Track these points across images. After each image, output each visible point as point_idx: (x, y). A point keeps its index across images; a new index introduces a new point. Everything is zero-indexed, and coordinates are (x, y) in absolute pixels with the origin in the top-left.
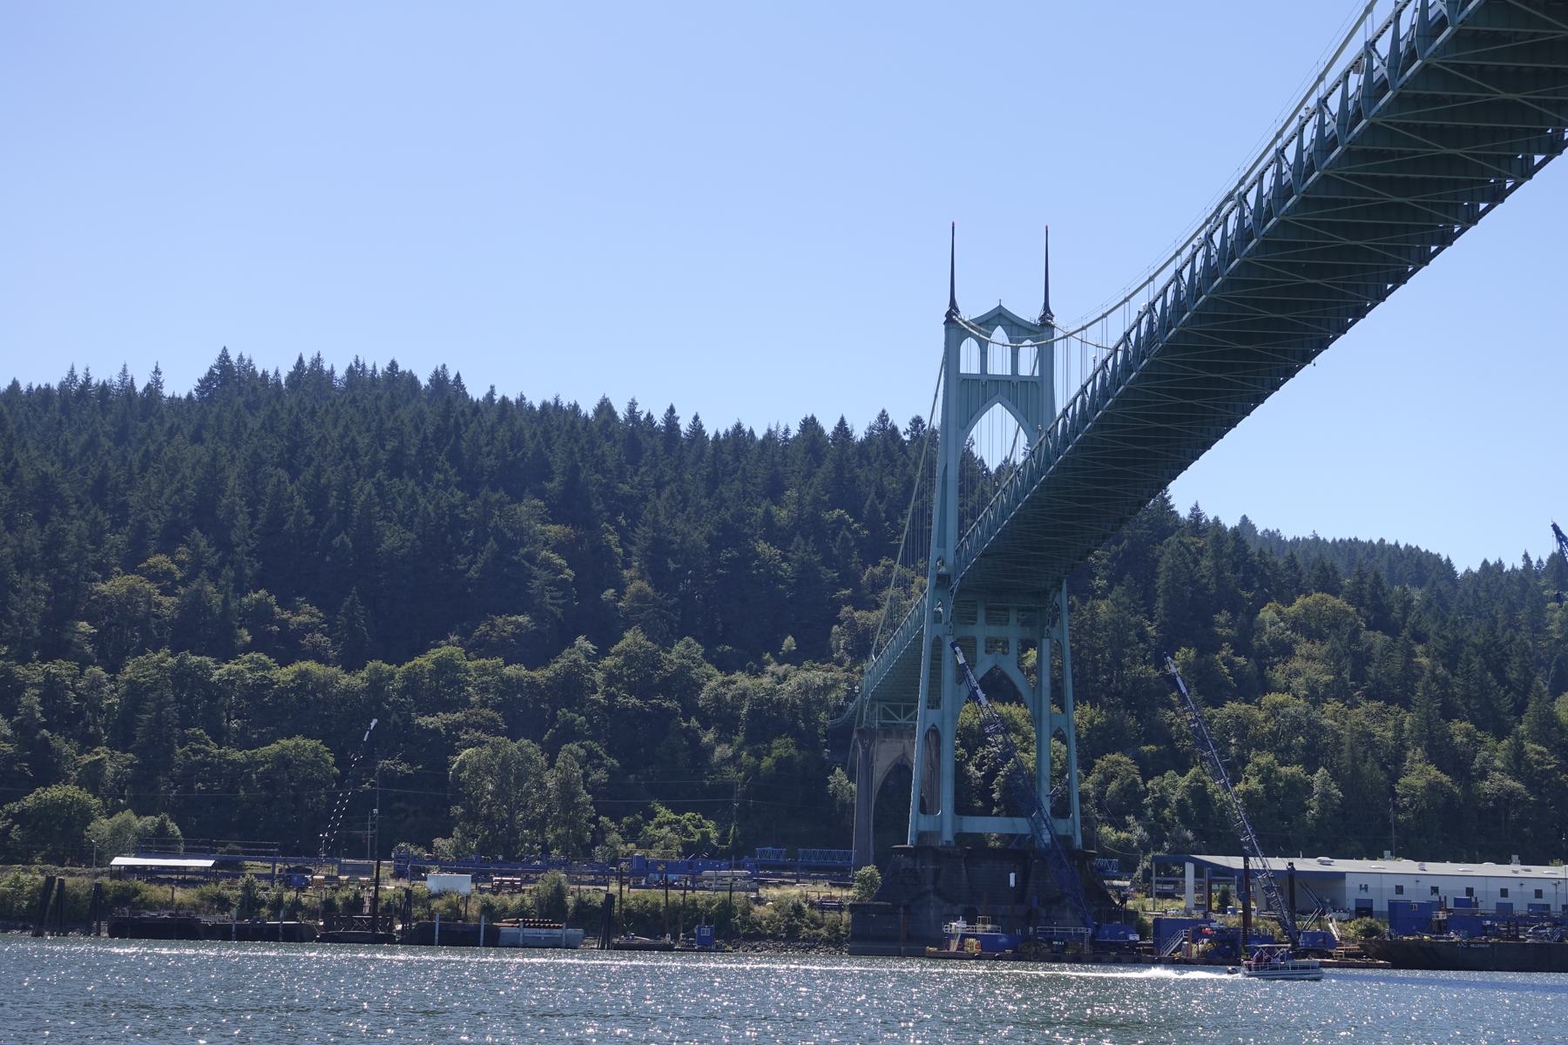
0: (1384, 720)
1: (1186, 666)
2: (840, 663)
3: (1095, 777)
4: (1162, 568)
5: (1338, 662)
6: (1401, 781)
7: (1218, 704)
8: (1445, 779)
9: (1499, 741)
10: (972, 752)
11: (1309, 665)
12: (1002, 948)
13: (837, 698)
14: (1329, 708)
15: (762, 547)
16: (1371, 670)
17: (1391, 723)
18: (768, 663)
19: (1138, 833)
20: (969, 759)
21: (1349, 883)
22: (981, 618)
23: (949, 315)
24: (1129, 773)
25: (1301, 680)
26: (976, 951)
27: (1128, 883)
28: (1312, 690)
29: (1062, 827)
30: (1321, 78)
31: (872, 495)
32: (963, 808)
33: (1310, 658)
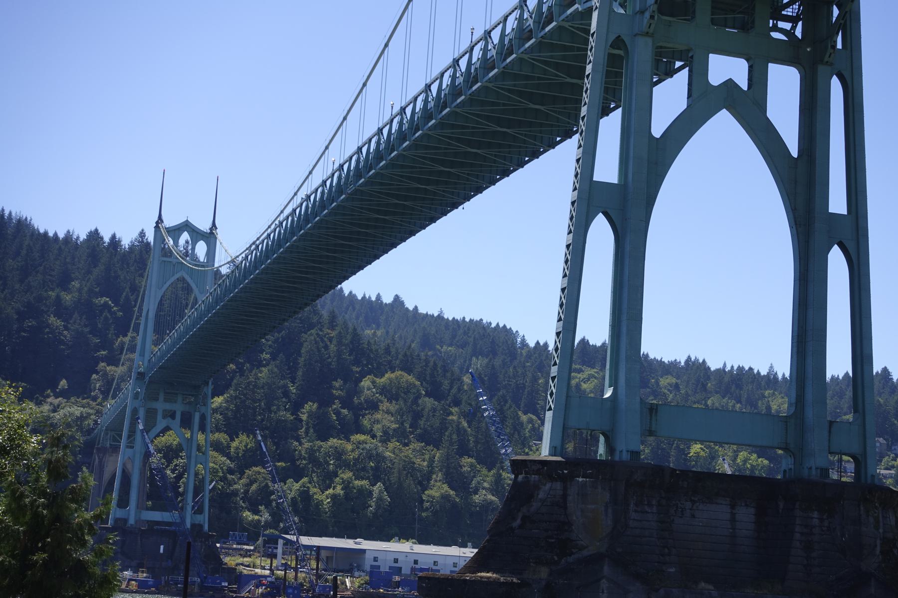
0: (423, 454)
1: (311, 415)
2: (95, 399)
3: (244, 481)
4: (303, 351)
5: (402, 416)
6: (426, 492)
7: (325, 439)
8: (452, 493)
9: (489, 471)
10: (169, 462)
11: (384, 418)
12: (149, 587)
13: (89, 425)
14: (391, 445)
15: (52, 319)
16: (422, 423)
17: (427, 457)
18: (48, 396)
19: (266, 516)
20: (167, 466)
21: (369, 557)
22: (161, 397)
23: (157, 223)
24: (265, 479)
25: (379, 426)
26: (135, 588)
27: (252, 548)
28: (385, 433)
29: (199, 519)
30: (282, 212)
31: (127, 290)
32: (140, 507)
33: (388, 412)
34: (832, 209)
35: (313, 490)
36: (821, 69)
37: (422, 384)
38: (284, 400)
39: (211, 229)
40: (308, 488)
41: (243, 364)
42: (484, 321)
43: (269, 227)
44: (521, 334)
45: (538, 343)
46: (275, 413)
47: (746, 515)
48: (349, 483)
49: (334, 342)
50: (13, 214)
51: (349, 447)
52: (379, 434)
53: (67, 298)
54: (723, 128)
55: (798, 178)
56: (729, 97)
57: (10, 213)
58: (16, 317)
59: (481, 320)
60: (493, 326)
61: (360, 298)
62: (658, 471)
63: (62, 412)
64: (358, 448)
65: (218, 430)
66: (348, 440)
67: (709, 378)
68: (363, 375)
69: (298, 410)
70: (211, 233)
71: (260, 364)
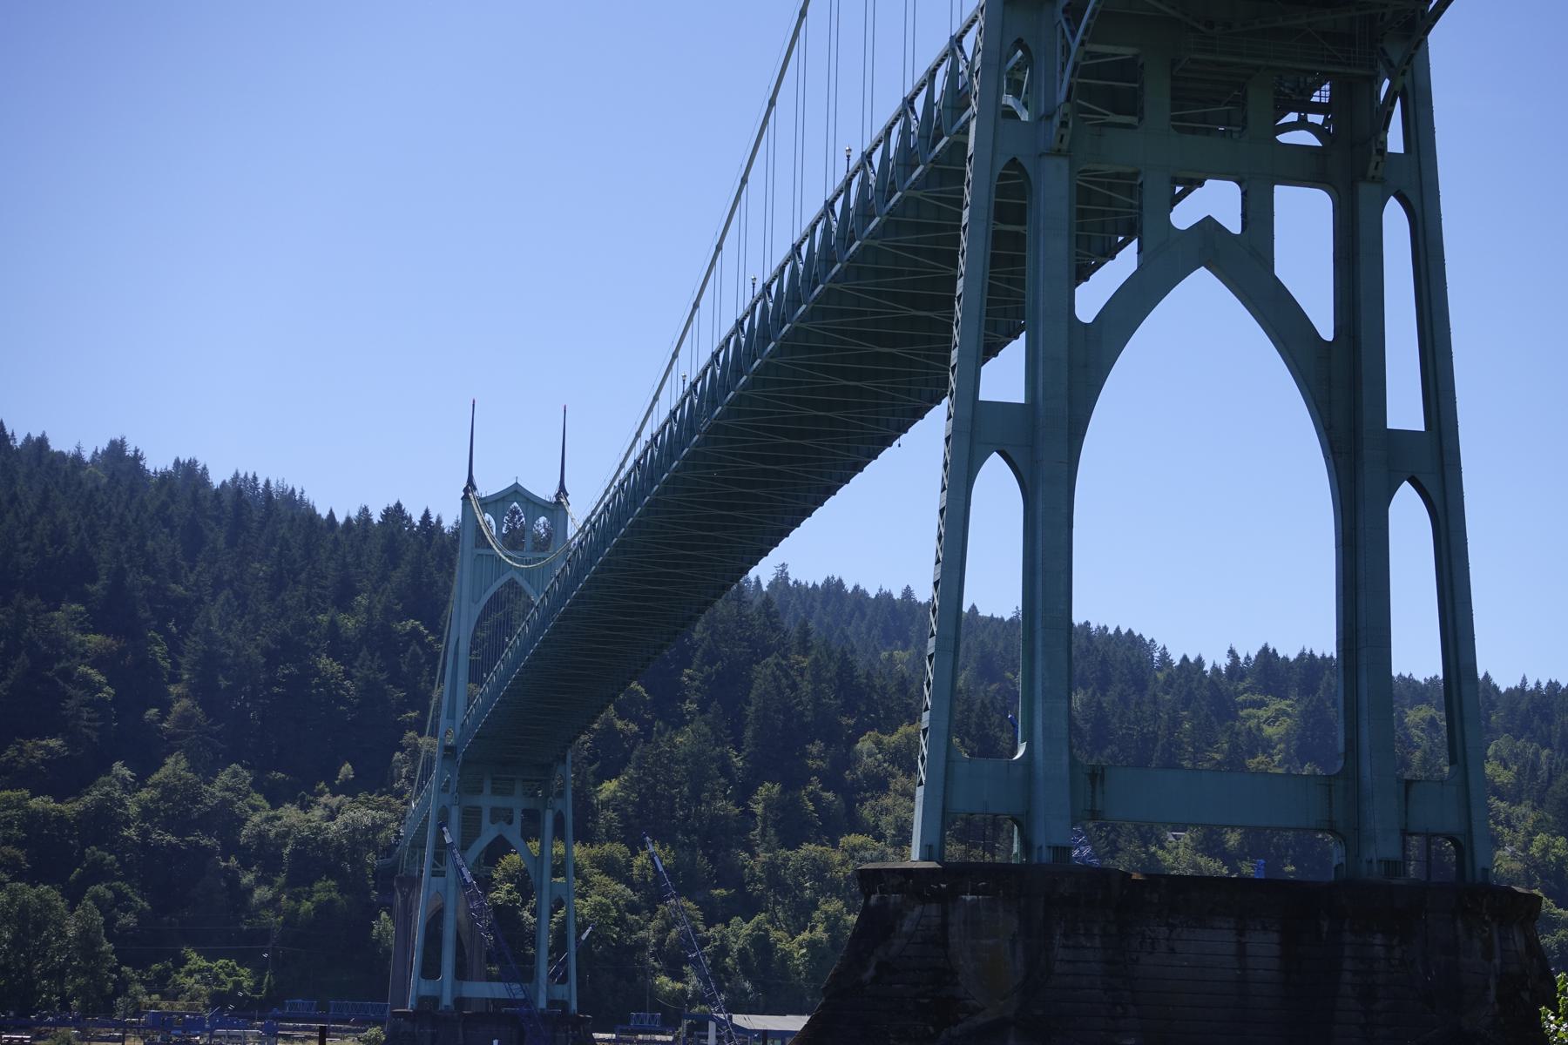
2: (399, 794)
7: (794, 845)
15: (324, 662)
18: (321, 793)
19: (693, 983)
20: (523, 905)
22: (487, 789)
23: (466, 490)
25: (890, 818)
29: (560, 992)
32: (461, 973)
34: (1393, 423)
35: (775, 935)
36: (1364, 189)
37: (962, 742)
38: (722, 780)
39: (558, 496)
40: (766, 930)
41: (651, 723)
42: (1093, 626)
43: (607, 492)
44: (1160, 645)
45: (1185, 658)
46: (708, 803)
47: (1264, 946)
48: (838, 919)
49: (807, 676)
50: (273, 484)
51: (837, 857)
52: (890, 832)
53: (349, 624)
54: (1201, 295)
55: (1336, 378)
56: (1207, 245)
57: (268, 482)
58: (263, 661)
59: (1087, 623)
60: (1111, 631)
61: (873, 596)
62: (1101, 877)
63: (340, 819)
64: (853, 858)
65: (612, 839)
66: (835, 845)
67: (1493, 706)
68: (860, 732)
69: (748, 797)
70: (558, 503)
71: (679, 722)
